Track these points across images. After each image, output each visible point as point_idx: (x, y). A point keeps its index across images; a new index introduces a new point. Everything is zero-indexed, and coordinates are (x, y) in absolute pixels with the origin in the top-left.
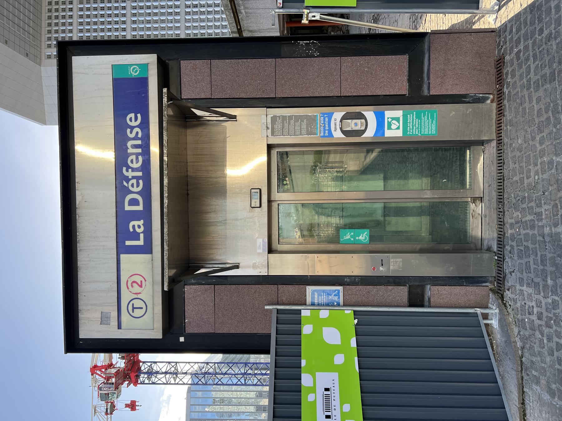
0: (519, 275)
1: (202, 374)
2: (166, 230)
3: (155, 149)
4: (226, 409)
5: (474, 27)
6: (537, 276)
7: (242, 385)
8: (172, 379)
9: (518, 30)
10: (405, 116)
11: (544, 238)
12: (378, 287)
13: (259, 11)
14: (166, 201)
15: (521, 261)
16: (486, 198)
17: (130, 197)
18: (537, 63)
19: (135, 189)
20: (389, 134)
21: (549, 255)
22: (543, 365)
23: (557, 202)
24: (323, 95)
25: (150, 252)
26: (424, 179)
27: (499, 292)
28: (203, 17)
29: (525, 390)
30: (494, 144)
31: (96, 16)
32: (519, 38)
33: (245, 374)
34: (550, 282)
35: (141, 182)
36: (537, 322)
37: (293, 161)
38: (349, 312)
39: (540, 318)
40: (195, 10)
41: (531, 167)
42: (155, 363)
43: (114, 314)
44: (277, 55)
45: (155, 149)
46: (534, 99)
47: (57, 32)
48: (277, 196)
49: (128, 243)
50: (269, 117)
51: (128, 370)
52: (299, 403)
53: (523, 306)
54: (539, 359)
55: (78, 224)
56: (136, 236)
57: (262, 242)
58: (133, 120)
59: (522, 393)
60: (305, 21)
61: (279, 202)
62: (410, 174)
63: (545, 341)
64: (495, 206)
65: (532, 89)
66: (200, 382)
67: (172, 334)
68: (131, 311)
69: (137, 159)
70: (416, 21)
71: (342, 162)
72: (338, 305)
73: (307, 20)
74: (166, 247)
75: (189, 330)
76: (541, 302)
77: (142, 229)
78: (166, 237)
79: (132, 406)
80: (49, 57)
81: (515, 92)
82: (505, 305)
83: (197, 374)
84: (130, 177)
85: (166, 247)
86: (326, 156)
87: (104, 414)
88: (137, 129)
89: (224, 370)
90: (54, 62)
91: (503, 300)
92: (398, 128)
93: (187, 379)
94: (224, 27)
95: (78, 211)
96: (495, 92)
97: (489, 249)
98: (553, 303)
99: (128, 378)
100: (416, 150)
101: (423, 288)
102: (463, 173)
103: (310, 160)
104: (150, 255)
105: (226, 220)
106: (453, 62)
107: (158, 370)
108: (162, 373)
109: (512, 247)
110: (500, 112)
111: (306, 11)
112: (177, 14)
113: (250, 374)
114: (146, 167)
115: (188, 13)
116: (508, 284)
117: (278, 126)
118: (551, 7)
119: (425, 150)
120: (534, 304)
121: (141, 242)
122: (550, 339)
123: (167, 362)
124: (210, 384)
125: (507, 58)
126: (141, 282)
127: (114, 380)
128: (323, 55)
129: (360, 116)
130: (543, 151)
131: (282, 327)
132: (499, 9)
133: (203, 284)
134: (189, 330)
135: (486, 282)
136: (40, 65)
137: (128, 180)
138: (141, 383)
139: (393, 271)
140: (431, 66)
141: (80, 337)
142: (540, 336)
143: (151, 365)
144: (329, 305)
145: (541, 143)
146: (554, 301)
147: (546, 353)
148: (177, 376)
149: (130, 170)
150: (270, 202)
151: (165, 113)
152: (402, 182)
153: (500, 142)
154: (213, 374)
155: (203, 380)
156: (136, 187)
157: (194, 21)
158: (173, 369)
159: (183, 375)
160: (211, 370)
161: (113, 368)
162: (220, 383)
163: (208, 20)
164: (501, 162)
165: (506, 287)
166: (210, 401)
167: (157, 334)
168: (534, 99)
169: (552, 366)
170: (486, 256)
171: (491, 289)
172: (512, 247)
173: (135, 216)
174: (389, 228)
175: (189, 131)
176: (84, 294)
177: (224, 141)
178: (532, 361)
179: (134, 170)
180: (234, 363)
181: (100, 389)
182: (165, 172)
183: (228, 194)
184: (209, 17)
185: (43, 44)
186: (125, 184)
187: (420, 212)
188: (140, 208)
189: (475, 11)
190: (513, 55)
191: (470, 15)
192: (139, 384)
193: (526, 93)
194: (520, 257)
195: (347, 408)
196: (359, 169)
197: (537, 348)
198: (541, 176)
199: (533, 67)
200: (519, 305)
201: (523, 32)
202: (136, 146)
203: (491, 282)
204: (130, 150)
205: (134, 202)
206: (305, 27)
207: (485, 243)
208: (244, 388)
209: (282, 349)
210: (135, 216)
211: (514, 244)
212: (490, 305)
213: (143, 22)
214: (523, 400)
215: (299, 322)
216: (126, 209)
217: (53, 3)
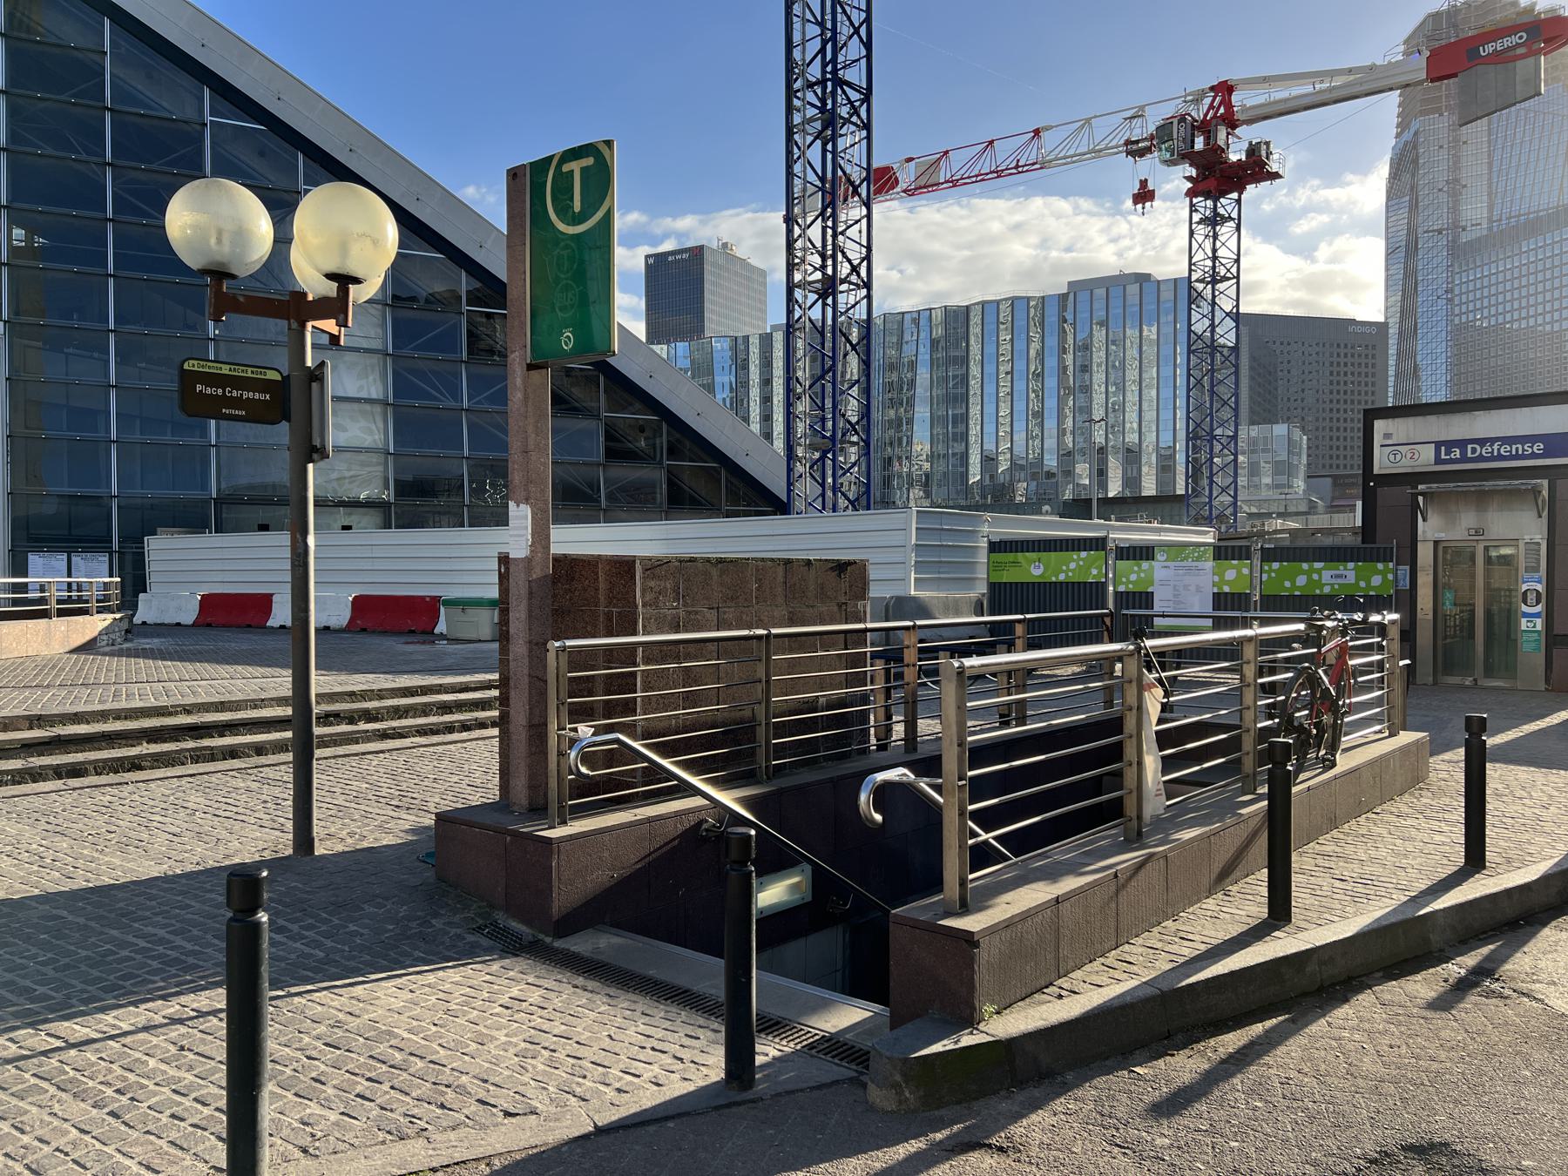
25: (1436, 464)
42: (1238, 228)
49: (1443, 448)
88: (1530, 450)
99: (1204, 174)
108: (1214, 250)
117: (1533, 547)
121: (1443, 457)
123: (1239, 255)
129: (1538, 602)
131: (1382, 550)
137: (1491, 446)
138: (1192, 205)
143: (1233, 219)
148: (1208, 283)
158: (1223, 272)
188: (1469, 455)
192: (1191, 201)
202: (1517, 449)
204: (1514, 447)
205: (1474, 451)
210: (1463, 453)
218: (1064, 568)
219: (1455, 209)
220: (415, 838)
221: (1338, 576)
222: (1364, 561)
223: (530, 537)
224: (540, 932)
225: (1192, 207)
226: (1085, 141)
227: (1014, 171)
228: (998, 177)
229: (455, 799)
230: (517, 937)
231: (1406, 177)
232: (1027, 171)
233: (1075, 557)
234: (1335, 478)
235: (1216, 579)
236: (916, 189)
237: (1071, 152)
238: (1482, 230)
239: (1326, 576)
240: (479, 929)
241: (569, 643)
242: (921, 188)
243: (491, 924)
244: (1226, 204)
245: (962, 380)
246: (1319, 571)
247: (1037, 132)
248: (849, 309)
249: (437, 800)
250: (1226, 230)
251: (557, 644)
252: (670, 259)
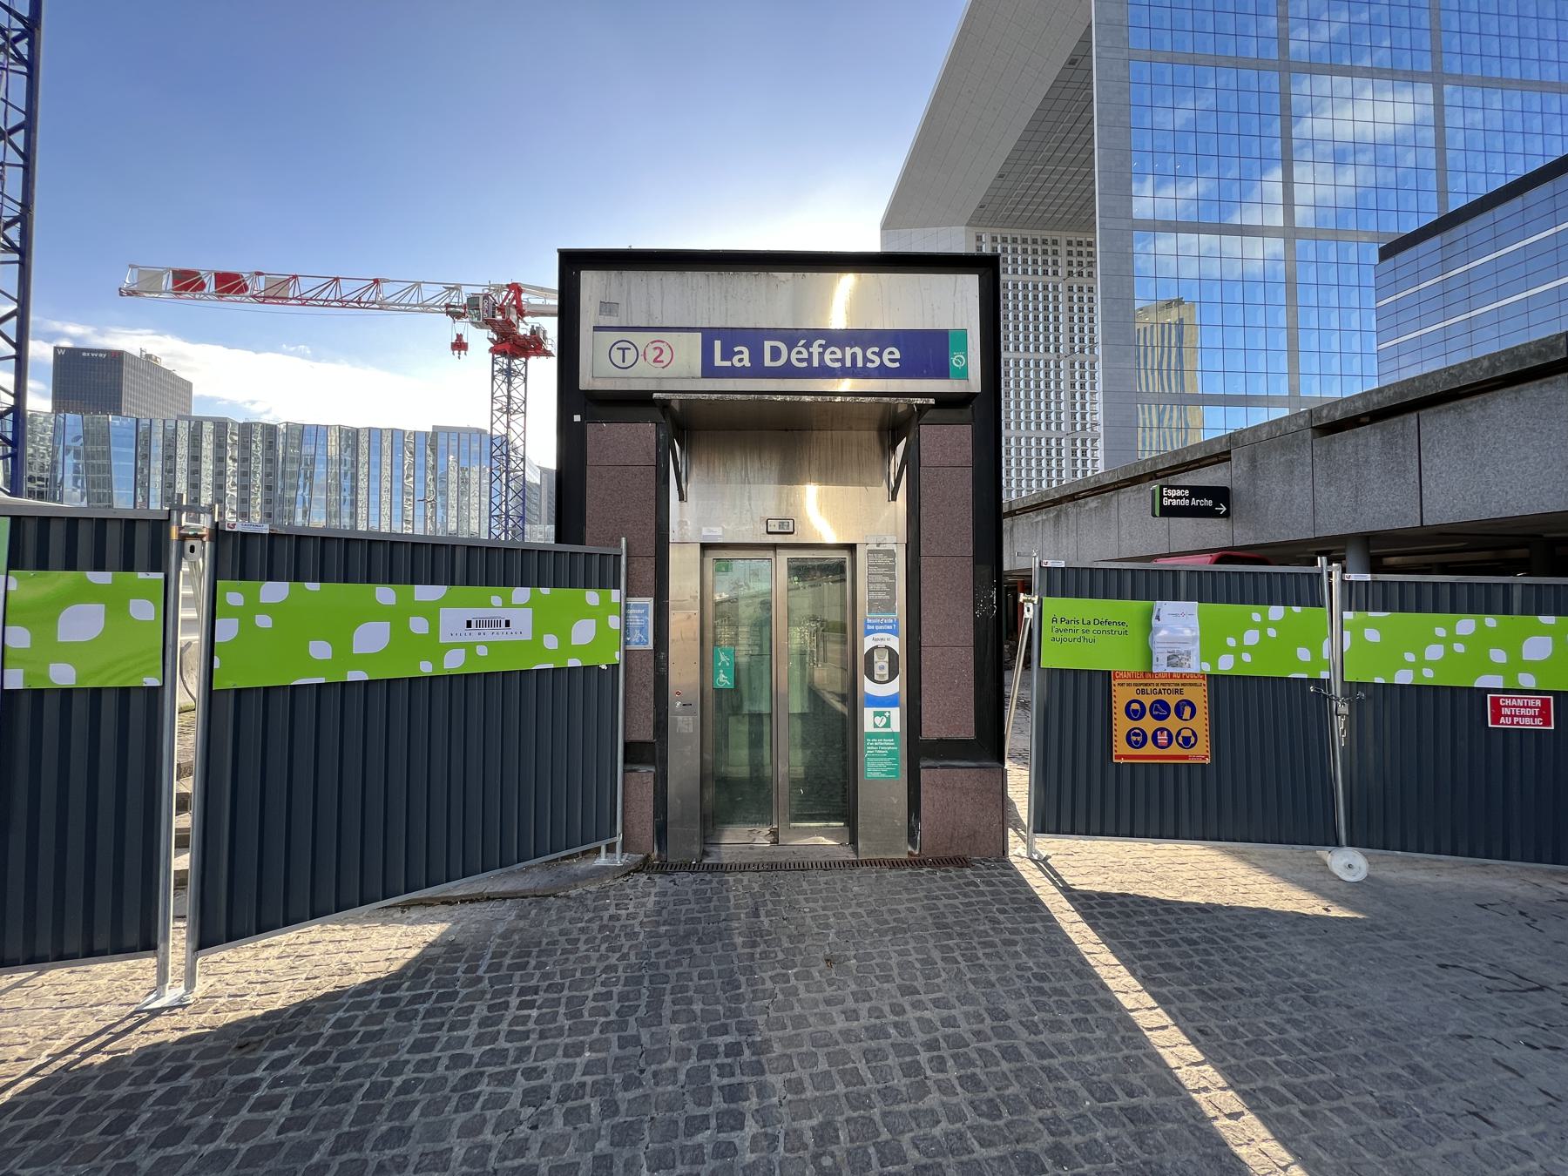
0: (670, 892)
1: (508, 451)
2: (739, 397)
3: (846, 385)
4: (453, 487)
5: (1010, 829)
6: (670, 913)
7: (490, 512)
8: (499, 406)
9: (1005, 884)
10: (892, 735)
11: (724, 920)
12: (652, 699)
13: (1039, 540)
14: (780, 398)
15: (690, 893)
16: (777, 849)
17: (782, 347)
18: (961, 906)
19: (794, 356)
20: (868, 714)
21: (700, 927)
22: (546, 923)
23: (774, 936)
24: (923, 623)
26: (803, 768)
27: (644, 866)
28: (1033, 463)
29: (508, 901)
30: (852, 857)
31: (1036, 309)
32: (994, 885)
33: (508, 516)
34: (663, 929)
35: (804, 364)
36: (606, 915)
37: (829, 588)
38: (617, 657)
39: (611, 918)
40: (1043, 451)
41: (820, 903)
42: (525, 380)
43: (614, 322)
44: (977, 559)
45: (846, 385)
46: (913, 905)
47: (1015, 251)
48: (783, 557)
49: (718, 344)
50: (894, 547)
51: (514, 340)
52: (488, 583)
53: (627, 897)
54: (554, 918)
55: (744, 273)
56: (727, 355)
57: (716, 534)
58: (892, 356)
59: (504, 897)
60: (1022, 597)
61: (773, 560)
62: (808, 752)
63: (580, 925)
64: (766, 860)
65: (926, 902)
66: (494, 448)
67: (586, 405)
68: (619, 345)
69: (837, 360)
70: (1019, 757)
71: (825, 660)
72: (627, 643)
73: (1024, 601)
74: (714, 397)
75: (591, 429)
76: (634, 918)
77: (738, 365)
78: (728, 397)
79: (459, 345)
80: (979, 238)
81: (923, 882)
82: (628, 874)
83: (508, 444)
84: (811, 350)
85: (714, 397)
86: (839, 639)
87: (447, 301)
88: (878, 362)
89: (512, 484)
90: (973, 250)
91: (634, 871)
92: (876, 726)
93: (500, 429)
94: (1019, 492)
95: (763, 274)
96: (922, 857)
97: (705, 854)
98: (634, 933)
100: (845, 758)
101: (652, 762)
102: (812, 818)
103: (833, 615)
104: (700, 375)
105: (749, 483)
106: (964, 800)
107: (514, 385)
108: (509, 392)
109: (710, 882)
110: (895, 864)
111: (1036, 599)
112: (1038, 426)
113: (507, 524)
114: (825, 372)
115: (1039, 440)
116: (657, 877)
117: (882, 560)
118: (1035, 922)
119: (845, 775)
120: (631, 910)
121: (718, 362)
122: (582, 930)
124: (491, 463)
125: (968, 871)
126: (662, 362)
127: (499, 318)
128: (976, 622)
129: (893, 674)
130: (843, 916)
131: (596, 562)
132: (1033, 860)
133: (657, 450)
134: (591, 429)
135: (659, 849)
136: (967, 225)
137: (808, 346)
138: (493, 359)
139: (676, 720)
140: (959, 770)
141: (582, 272)
142: (586, 918)
144: (626, 629)
145: (853, 915)
146: (636, 935)
147: (563, 926)
149: (821, 350)
150: (774, 547)
151: (901, 400)
152: (798, 740)
153: (854, 864)
154: (507, 467)
155: (498, 452)
156: (797, 357)
157: (1028, 450)
158: (515, 407)
159: (505, 423)
160: (513, 465)
161: (519, 318)
162: (494, 478)
163: (1029, 471)
164: (828, 866)
165: (653, 876)
166: (464, 463)
167: (586, 382)
168: (913, 905)
169: (544, 933)
170: (697, 849)
171: (649, 856)
172: (710, 882)
173: (757, 355)
174: (732, 719)
175: (874, 434)
176: (645, 278)
177: (860, 484)
178: (549, 909)
179: (821, 355)
180: (523, 500)
181: (486, 297)
182: (820, 399)
183: (786, 487)
184: (1034, 471)
185: (997, 230)
186: (802, 342)
187: (756, 766)
188: (768, 362)
189: (1031, 828)
190: (972, 878)
191: (1026, 823)
193: (922, 894)
194: (695, 892)
195: (482, 651)
196: (816, 684)
197: (568, 915)
198: (809, 915)
199: (956, 902)
200: (628, 891)
201: (1002, 889)
203: (659, 856)
204: (848, 351)
205: (776, 353)
206: (1016, 597)
207: (713, 849)
208: (487, 514)
209: (565, 561)
210: (757, 355)
211: (714, 885)
212: (626, 855)
213: (1027, 376)
214: (493, 899)
215: (602, 585)
216: (766, 342)
217: (1055, 248)
218: (1231, 642)
222: (556, 584)
225: (494, 361)
226: (415, 297)
228: (343, 307)
233: (1246, 657)
237: (405, 301)
239: (452, 620)
242: (269, 297)
244: (518, 363)
246: (431, 612)
247: (376, 281)
252: (84, 354)
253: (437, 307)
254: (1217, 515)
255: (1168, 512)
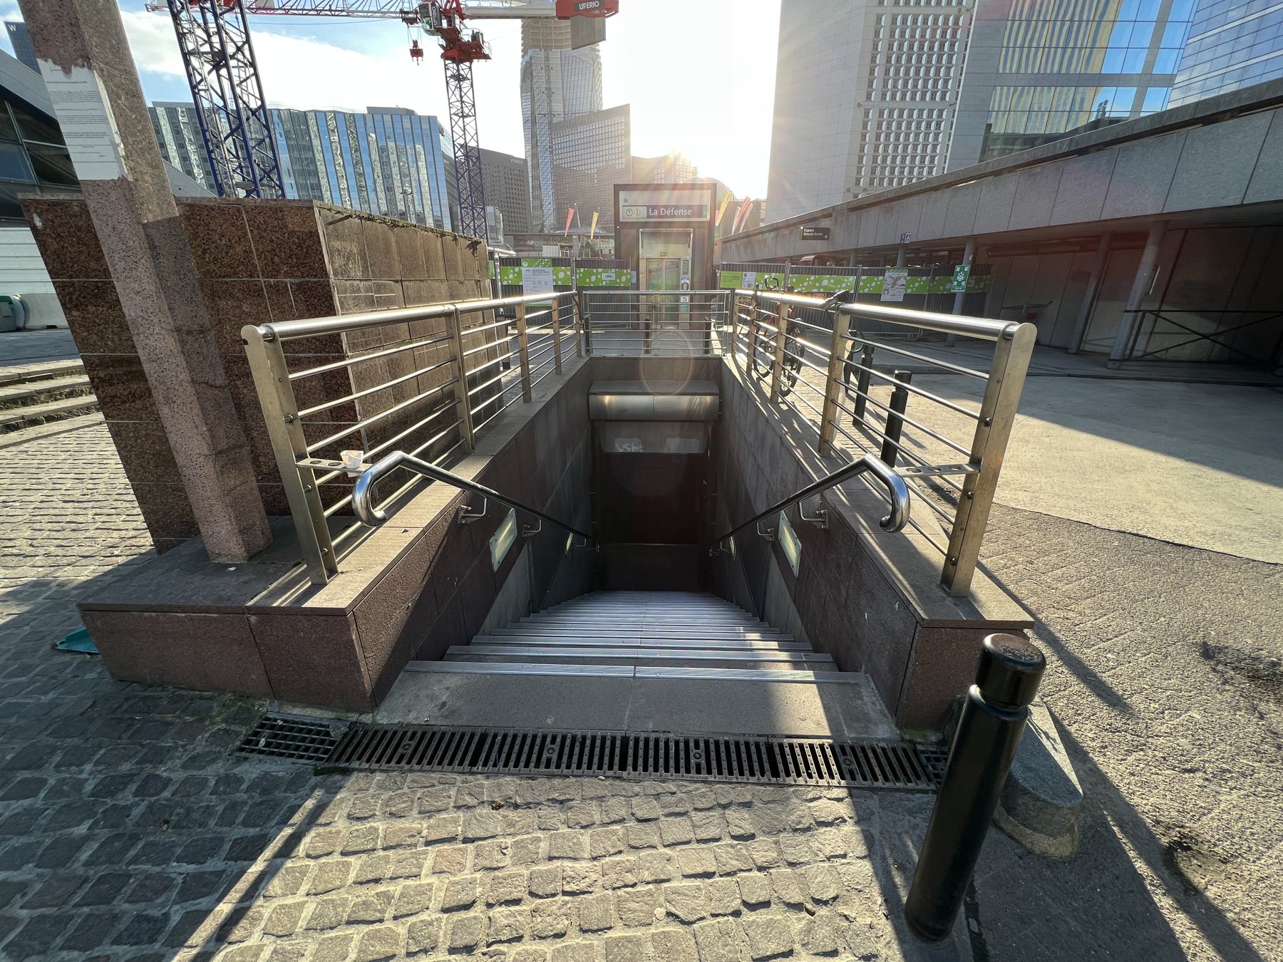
79: (416, 52)
108: (461, 97)
159: (462, 126)
219: (550, 104)
220: (25, 609)
221: (608, 276)
223: (118, 139)
224: (348, 711)
227: (329, 13)
229: (57, 526)
230: (318, 733)
231: (528, 82)
232: (338, 15)
234: (515, 236)
235: (555, 277)
236: (257, 9)
238: (561, 119)
240: (249, 745)
241: (280, 327)
242: (260, 9)
243: (262, 726)
245: (311, 162)
248: (241, 82)
249: (28, 533)
250: (465, 84)
251: (262, 330)
253: (392, 12)
254: (824, 239)
255: (804, 238)
